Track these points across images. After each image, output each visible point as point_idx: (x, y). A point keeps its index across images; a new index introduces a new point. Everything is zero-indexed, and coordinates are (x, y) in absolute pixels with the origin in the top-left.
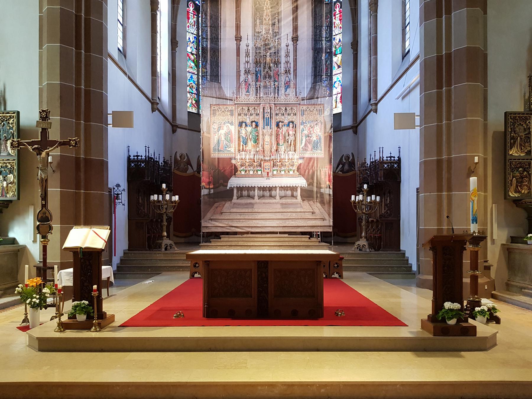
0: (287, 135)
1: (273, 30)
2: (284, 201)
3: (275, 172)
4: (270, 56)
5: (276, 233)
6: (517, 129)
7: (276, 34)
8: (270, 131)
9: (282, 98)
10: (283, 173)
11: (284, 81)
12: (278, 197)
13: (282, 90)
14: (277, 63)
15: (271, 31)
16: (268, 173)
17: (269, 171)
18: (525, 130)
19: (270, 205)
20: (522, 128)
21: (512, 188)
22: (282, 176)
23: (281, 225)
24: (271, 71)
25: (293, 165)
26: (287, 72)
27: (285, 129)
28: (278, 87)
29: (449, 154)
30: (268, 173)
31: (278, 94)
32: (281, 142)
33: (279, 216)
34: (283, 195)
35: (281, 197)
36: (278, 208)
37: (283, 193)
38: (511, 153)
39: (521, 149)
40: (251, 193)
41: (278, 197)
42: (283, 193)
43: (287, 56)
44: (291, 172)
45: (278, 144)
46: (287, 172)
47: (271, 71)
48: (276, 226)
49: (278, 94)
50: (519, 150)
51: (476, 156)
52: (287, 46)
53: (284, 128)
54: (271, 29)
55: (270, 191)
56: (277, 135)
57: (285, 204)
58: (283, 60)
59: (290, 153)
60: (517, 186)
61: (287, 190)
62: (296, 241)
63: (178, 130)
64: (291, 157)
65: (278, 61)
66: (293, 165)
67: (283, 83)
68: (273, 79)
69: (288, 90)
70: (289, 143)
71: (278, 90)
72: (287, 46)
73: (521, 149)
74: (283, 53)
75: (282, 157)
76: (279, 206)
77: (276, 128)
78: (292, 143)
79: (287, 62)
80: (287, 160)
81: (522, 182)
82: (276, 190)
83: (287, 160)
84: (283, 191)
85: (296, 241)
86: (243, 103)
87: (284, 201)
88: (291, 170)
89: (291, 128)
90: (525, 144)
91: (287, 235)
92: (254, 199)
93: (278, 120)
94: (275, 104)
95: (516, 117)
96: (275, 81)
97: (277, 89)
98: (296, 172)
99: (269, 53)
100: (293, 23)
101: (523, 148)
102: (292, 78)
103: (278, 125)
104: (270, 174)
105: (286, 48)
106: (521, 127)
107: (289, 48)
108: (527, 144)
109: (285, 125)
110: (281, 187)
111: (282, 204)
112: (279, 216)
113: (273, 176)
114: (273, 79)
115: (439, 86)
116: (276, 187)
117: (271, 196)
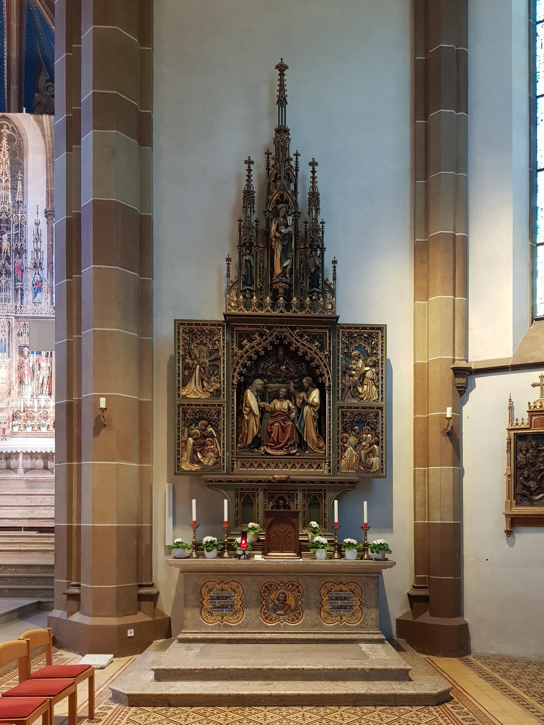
0: (37, 367)
1: (13, 197)
2: (30, 476)
3: (16, 429)
4: (9, 239)
5: (18, 529)
6: (196, 352)
7: (18, 205)
8: (8, 361)
9: (29, 307)
10: (29, 429)
11: (31, 280)
12: (21, 470)
13: (29, 296)
14: (20, 252)
15: (10, 201)
16: (4, 429)
17: (5, 426)
18: (211, 353)
19: (7, 482)
20: (205, 349)
21: (186, 456)
22: (27, 435)
23: (26, 516)
24: (9, 264)
25: (46, 418)
26: (37, 266)
27: (33, 358)
28: (22, 290)
29: (80, 395)
30: (4, 429)
31: (22, 303)
32: (27, 380)
33: (22, 501)
34: (29, 467)
35: (26, 470)
36: (22, 488)
37: (29, 463)
38: (184, 393)
39: (203, 387)
40: (13, 463)
41: (21, 470)
42: (29, 463)
43: (37, 240)
44: (44, 429)
45: (21, 382)
46: (36, 428)
47: (9, 264)
48: (18, 517)
49: (22, 303)
50: (199, 388)
51: (103, 396)
52: (37, 224)
53: (31, 356)
54: (10, 197)
55: (6, 459)
56: (20, 367)
57: (33, 481)
58: (30, 246)
59: (42, 397)
60: (195, 452)
61: (37, 459)
62: (33, 543)
63: (479, 381)
64: (43, 404)
65: (22, 249)
66: (46, 418)
67: (30, 284)
68: (13, 276)
69: (39, 295)
70: (40, 381)
71: (22, 295)
72: (37, 224)
73: (203, 387)
74: (30, 237)
75: (29, 404)
76: (23, 484)
77: (18, 357)
78: (45, 382)
79: (37, 251)
80: (36, 410)
81: (204, 444)
82: (17, 458)
83: (36, 410)
84: (29, 460)
85: (33, 543)
86: (31, 315)
87: (30, 476)
88: (43, 425)
89: (44, 358)
90: (209, 378)
91: (34, 533)
92: (16, 472)
93: (22, 344)
94: (16, 318)
95: (378, 339)
96: (16, 280)
97: (20, 292)
98: (51, 428)
99: (6, 235)
100: (47, 187)
101: (205, 384)
102: (45, 276)
103: (21, 353)
104: (8, 432)
105: (35, 227)
106: (202, 347)
107: (40, 227)
108: (213, 378)
109: (32, 353)
110: (27, 453)
111: (27, 481)
112: (22, 501)
113: (13, 434)
114: (13, 276)
115: (69, 276)
116: (17, 453)
117: (9, 468)
